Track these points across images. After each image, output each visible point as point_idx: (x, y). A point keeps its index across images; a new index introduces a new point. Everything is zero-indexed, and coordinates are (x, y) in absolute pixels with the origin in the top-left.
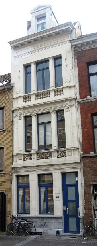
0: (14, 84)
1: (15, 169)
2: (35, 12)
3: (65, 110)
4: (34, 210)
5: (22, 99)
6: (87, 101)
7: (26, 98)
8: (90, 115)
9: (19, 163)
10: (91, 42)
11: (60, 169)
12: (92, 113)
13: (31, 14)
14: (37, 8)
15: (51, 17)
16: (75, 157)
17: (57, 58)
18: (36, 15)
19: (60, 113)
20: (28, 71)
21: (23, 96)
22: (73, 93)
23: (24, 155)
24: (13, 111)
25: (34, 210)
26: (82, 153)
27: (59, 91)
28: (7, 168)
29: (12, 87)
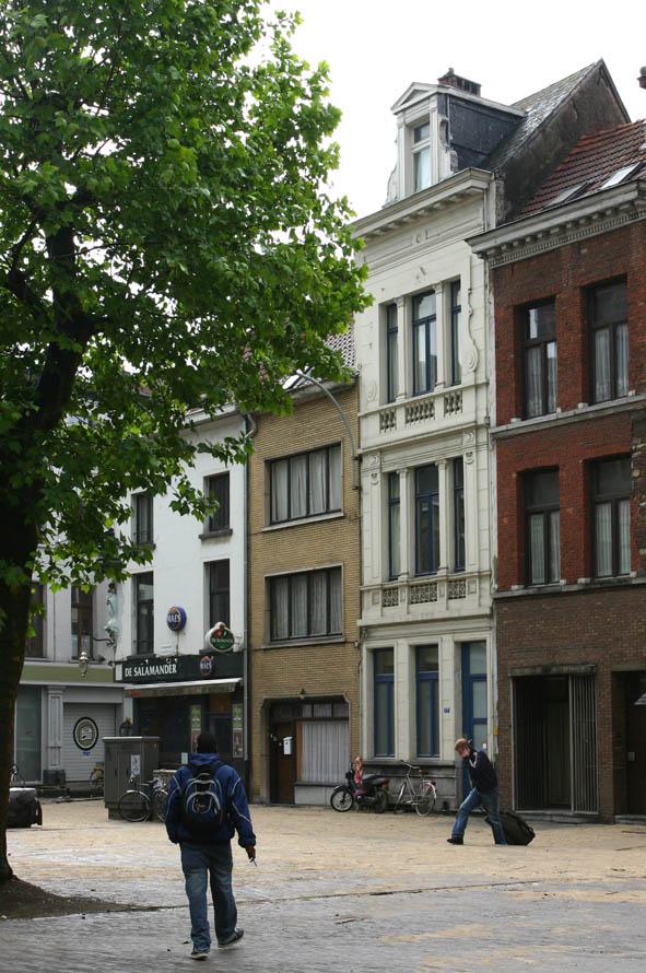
0: (303, 693)
1: (366, 631)
2: (404, 110)
3: (465, 459)
4: (403, 750)
5: (377, 418)
6: (510, 433)
7: (387, 420)
8: (514, 475)
9: (373, 614)
10: (595, 217)
11: (453, 632)
12: (520, 469)
13: (396, 114)
14: (409, 93)
15: (85, 921)
16: (480, 599)
17: (453, 285)
18: (408, 121)
19: (457, 465)
20: (474, 670)
21: (379, 412)
22: (480, 406)
23: (384, 590)
24: (359, 459)
25: (403, 750)
26: (496, 586)
27: (453, 402)
28: (349, 627)
29: (357, 378)
